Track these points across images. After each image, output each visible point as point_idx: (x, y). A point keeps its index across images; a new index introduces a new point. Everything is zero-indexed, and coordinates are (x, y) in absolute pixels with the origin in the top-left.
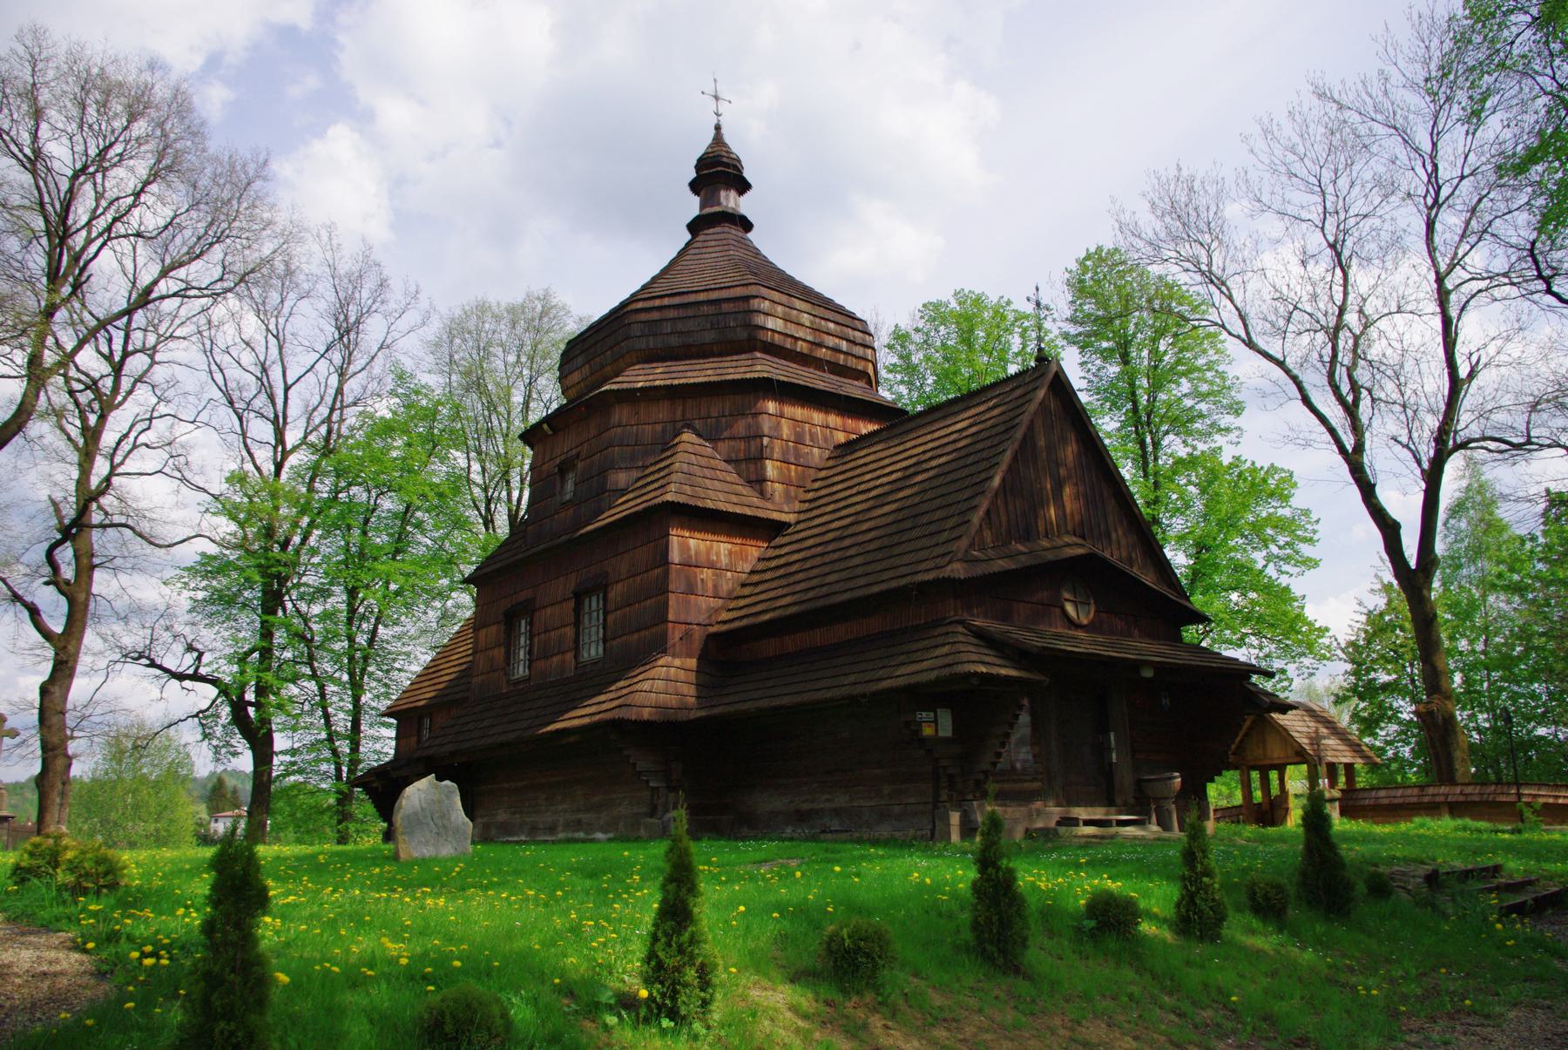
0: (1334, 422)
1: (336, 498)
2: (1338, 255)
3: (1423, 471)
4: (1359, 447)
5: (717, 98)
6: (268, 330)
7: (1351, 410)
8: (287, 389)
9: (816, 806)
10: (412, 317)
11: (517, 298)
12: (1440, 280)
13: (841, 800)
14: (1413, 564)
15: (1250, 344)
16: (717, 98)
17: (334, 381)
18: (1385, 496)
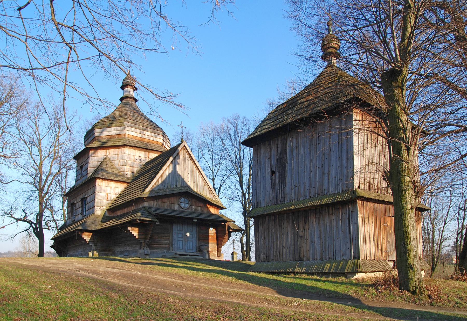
10: (76, 119)
13: (128, 248)
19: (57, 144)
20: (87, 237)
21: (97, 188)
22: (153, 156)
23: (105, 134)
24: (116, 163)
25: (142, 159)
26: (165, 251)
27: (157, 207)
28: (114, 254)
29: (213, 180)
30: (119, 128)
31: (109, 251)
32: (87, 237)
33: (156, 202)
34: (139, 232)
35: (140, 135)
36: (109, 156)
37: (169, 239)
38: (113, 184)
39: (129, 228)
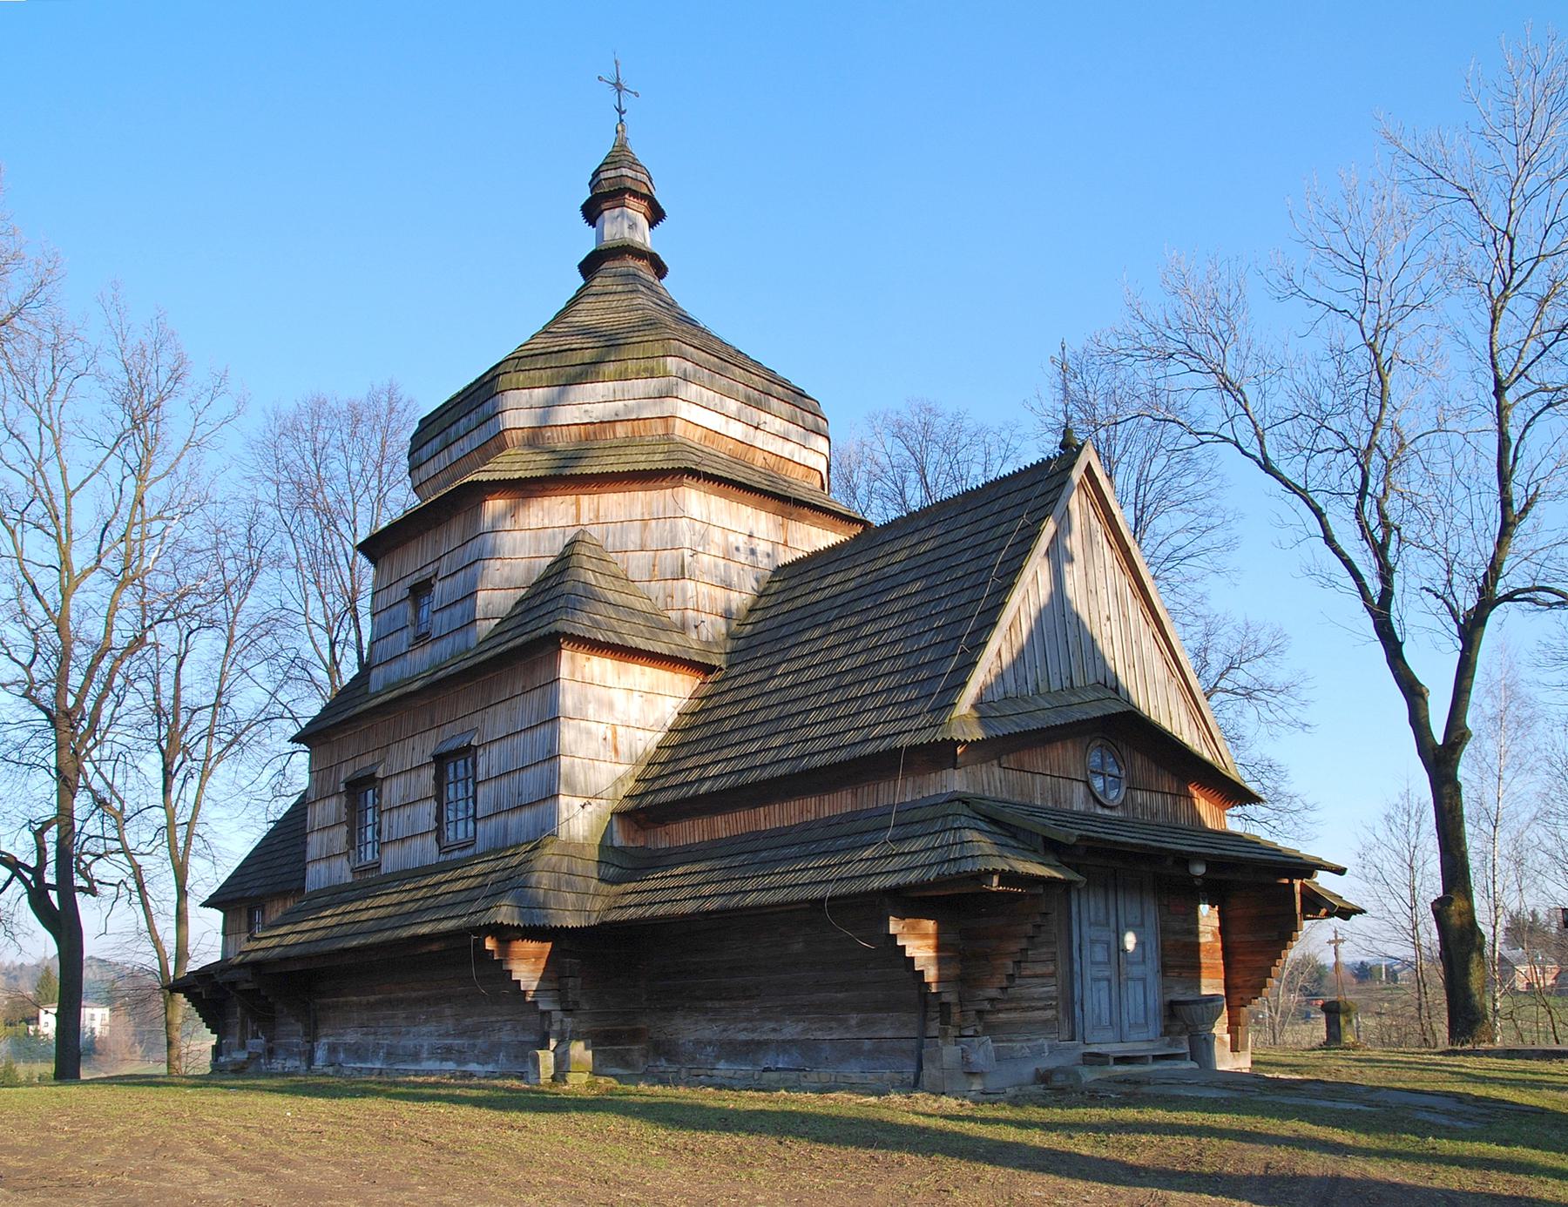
0: (1362, 569)
1: (143, 637)
2: (1377, 356)
3: (1460, 627)
4: (1386, 595)
5: (618, 86)
6: (41, 421)
7: (1380, 550)
8: (69, 495)
9: (756, 1036)
10: (223, 406)
11: (359, 393)
12: (1499, 389)
13: (791, 1030)
14: (1440, 741)
15: (1267, 466)
16: (618, 86)
17: (130, 485)
18: (1412, 655)
19: (138, 519)
20: (527, 968)
21: (569, 695)
22: (816, 537)
23: (567, 415)
24: (637, 564)
25: (763, 547)
26: (1044, 1042)
27: (1005, 796)
28: (665, 1050)
29: (1470, 630)
30: (640, 386)
31: (635, 1036)
32: (527, 968)
33: (997, 770)
34: (939, 948)
35: (737, 430)
36: (595, 532)
37: (1052, 975)
38: (642, 675)
39: (894, 926)
